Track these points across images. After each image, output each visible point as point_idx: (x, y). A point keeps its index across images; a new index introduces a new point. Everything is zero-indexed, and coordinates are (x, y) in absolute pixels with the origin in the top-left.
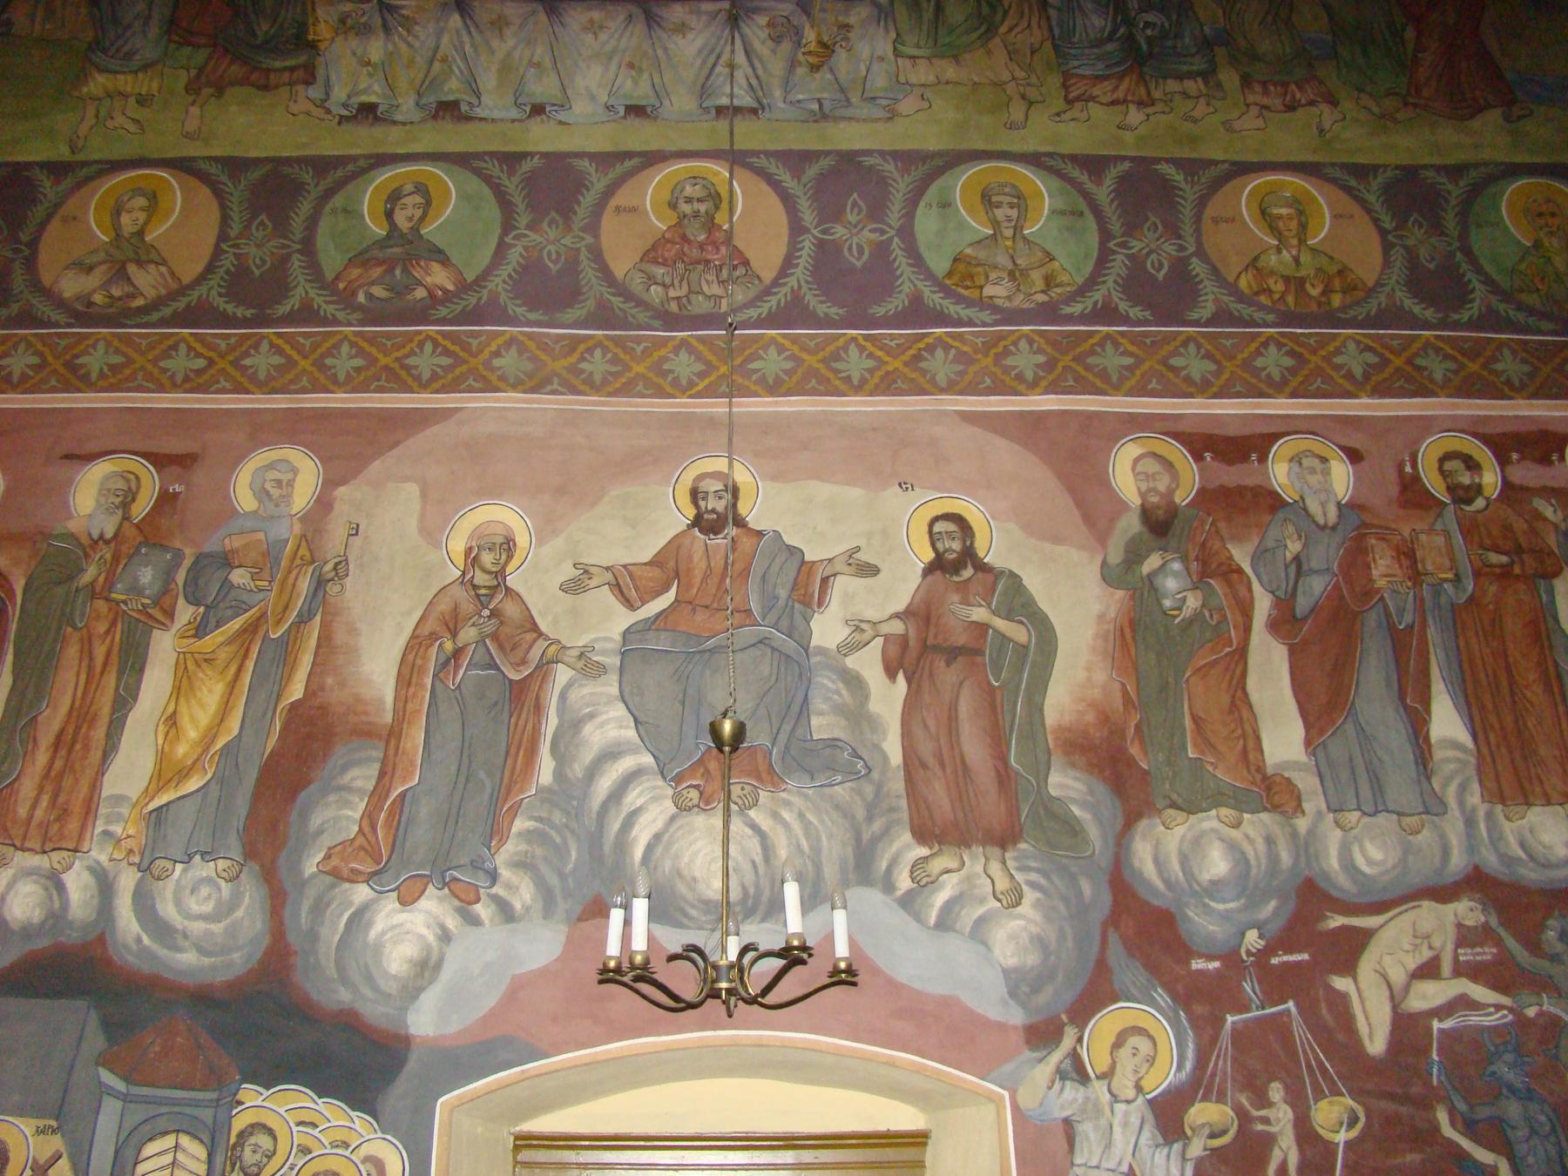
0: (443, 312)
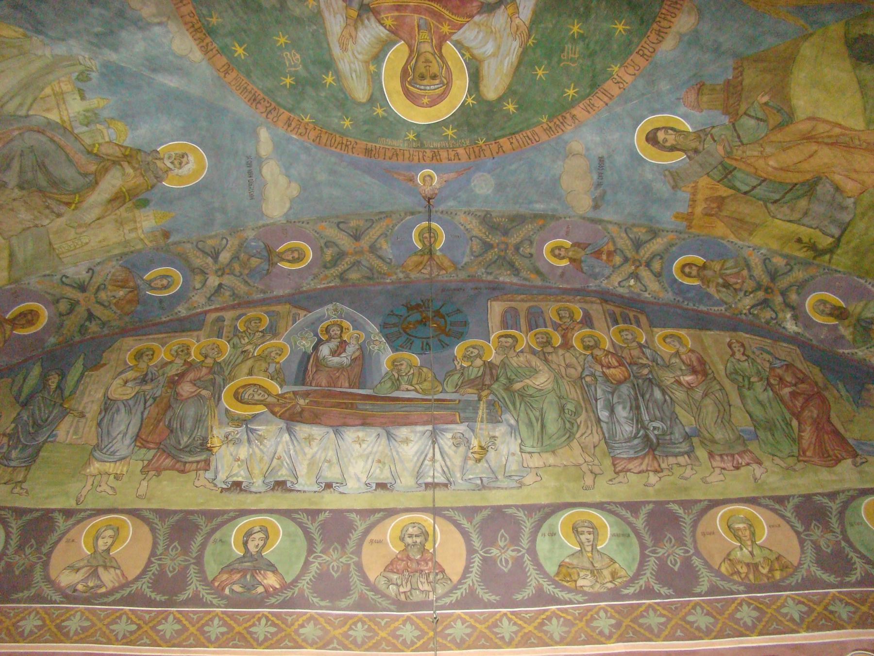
0: (273, 600)
